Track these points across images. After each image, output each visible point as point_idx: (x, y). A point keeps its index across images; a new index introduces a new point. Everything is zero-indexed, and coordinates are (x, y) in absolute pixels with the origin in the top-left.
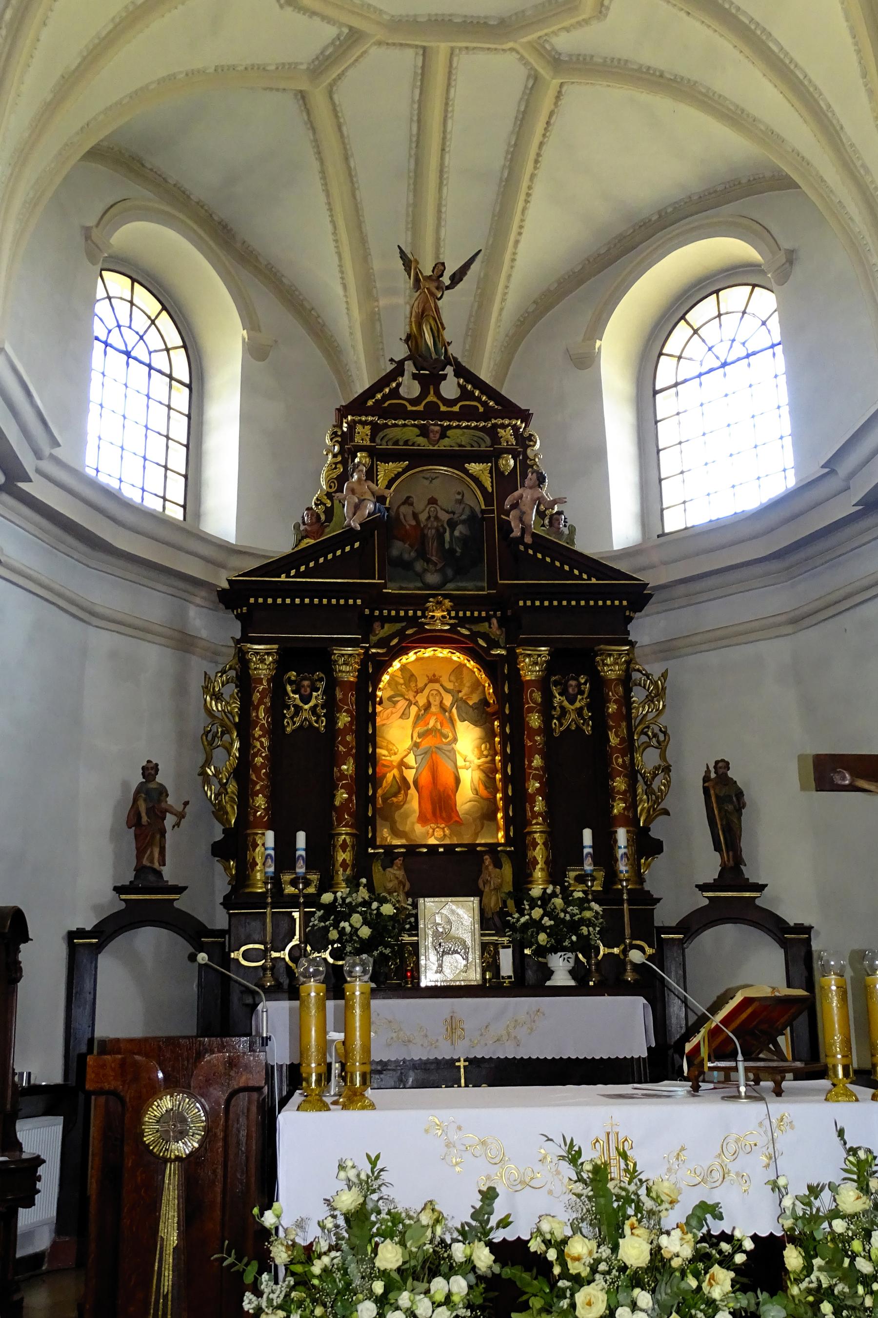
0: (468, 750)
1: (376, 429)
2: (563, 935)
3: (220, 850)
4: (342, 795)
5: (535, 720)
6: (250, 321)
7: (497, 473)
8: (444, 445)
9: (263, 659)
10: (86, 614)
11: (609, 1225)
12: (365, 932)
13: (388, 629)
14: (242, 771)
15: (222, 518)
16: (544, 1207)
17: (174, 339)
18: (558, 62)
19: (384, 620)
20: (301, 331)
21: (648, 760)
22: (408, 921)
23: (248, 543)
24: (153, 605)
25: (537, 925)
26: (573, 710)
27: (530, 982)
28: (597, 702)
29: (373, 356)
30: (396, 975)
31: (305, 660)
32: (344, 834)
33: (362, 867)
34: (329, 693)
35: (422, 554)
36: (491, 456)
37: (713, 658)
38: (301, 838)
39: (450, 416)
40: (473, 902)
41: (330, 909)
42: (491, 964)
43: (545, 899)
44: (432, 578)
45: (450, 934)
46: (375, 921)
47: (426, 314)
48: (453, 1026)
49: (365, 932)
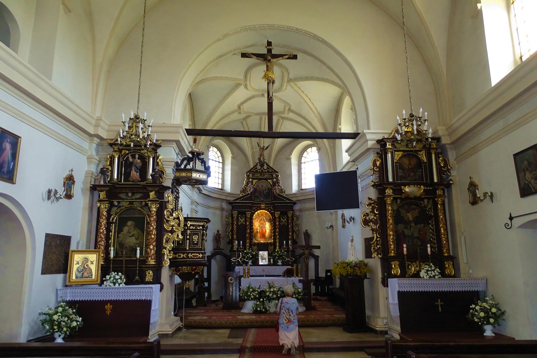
0: (268, 226)
1: (253, 175)
2: (280, 257)
3: (228, 243)
4: (247, 235)
5: (277, 223)
6: (233, 153)
7: (273, 182)
8: (264, 177)
9: (235, 213)
10: (209, 207)
11: (270, 287)
12: (251, 256)
13: (255, 208)
14: (232, 231)
15: (228, 188)
16: (265, 288)
17: (219, 155)
18: (282, 118)
19: (254, 207)
20: (241, 153)
21: (296, 229)
22: (257, 255)
23: (233, 192)
24: (217, 204)
25: (276, 256)
26: (284, 220)
27: (275, 264)
28: (288, 220)
29: (254, 161)
30: (255, 262)
31: (242, 213)
32: (248, 241)
33: (250, 246)
34: (245, 218)
35: (260, 195)
36: (272, 179)
37: (307, 212)
38: (241, 242)
39: (265, 172)
40: (267, 252)
41: (246, 253)
42: (269, 261)
43: (278, 251)
44: (262, 199)
45: (264, 257)
46: (252, 255)
47: (261, 155)
48: (263, 270)
49: (251, 256)
